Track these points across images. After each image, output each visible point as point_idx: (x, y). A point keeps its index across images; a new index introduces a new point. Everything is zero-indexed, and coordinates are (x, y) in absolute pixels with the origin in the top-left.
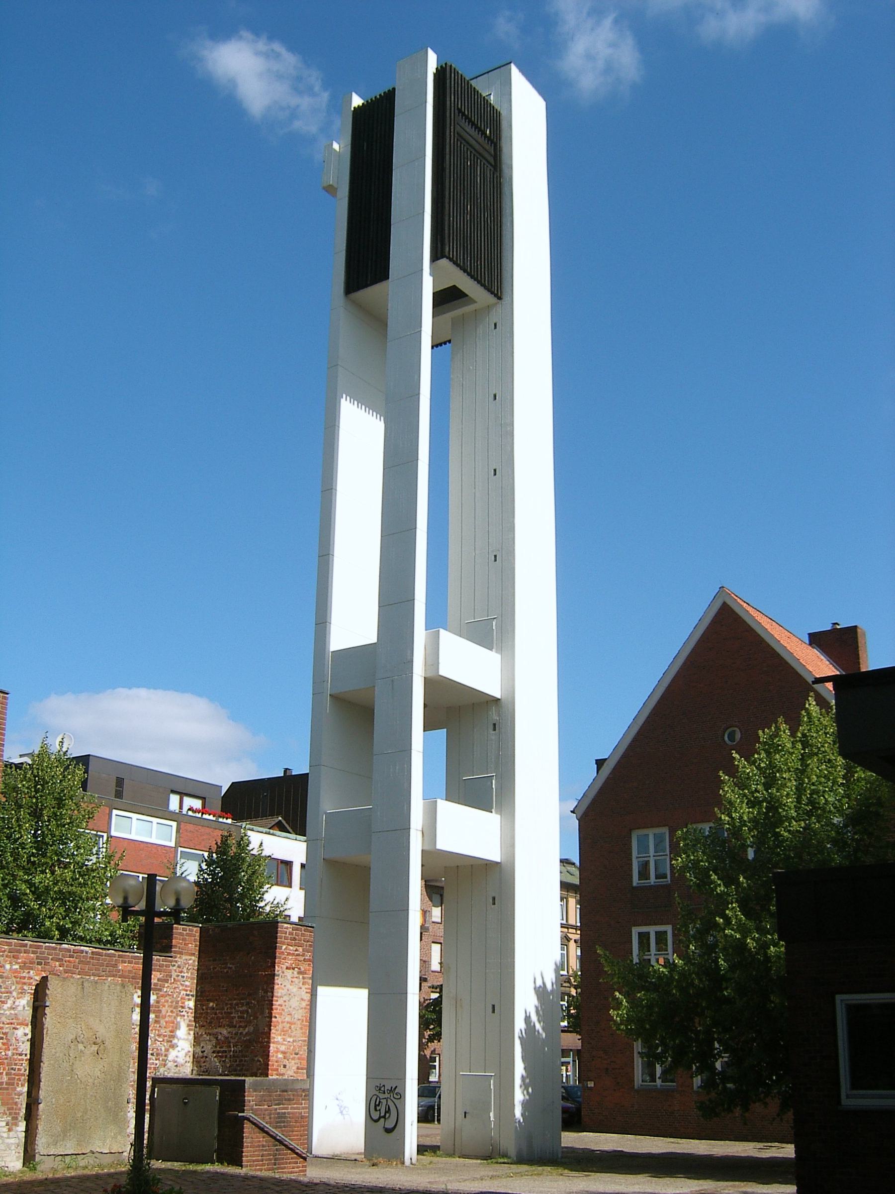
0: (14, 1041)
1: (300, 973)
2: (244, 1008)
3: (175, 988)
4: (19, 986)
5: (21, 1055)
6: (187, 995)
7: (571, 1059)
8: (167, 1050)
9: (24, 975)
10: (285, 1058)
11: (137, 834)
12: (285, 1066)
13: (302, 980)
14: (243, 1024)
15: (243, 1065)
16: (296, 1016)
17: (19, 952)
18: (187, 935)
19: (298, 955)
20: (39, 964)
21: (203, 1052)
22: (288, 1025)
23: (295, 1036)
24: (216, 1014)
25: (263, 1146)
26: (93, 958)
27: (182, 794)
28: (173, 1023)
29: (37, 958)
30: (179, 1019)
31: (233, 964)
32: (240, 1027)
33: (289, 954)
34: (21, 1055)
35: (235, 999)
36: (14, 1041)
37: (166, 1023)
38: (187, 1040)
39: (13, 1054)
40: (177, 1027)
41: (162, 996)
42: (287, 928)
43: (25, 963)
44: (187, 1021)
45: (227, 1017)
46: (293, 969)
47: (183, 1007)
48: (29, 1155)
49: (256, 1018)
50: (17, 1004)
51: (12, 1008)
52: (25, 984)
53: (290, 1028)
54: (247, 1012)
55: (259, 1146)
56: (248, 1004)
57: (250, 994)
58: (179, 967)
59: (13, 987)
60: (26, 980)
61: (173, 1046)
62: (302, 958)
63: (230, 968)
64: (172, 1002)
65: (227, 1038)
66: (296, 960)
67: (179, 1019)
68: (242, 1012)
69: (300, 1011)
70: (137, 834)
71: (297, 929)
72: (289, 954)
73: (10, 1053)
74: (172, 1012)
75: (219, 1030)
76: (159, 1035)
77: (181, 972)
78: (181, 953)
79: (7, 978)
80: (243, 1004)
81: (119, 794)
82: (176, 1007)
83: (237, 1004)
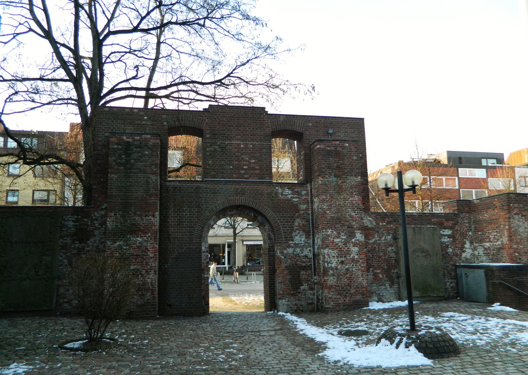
0: (388, 252)
1: (523, 216)
2: (495, 234)
3: (461, 227)
4: (386, 231)
5: (392, 258)
6: (468, 230)
7: (474, 190)
8: (461, 253)
9: (389, 226)
10: (520, 255)
11: (469, 175)
12: (520, 259)
13: (524, 219)
14: (495, 241)
15: (498, 259)
16: (523, 236)
17: (385, 218)
18: (464, 204)
19: (520, 208)
20: (395, 222)
21: (479, 253)
22: (519, 240)
23: (524, 245)
24: (482, 237)
25: (511, 296)
26: (419, 218)
27: (487, 158)
28: (462, 242)
29: (393, 219)
30: (465, 240)
31: (487, 215)
32: (494, 242)
33: (515, 208)
34: (392, 258)
35: (490, 230)
36: (388, 252)
37: (459, 242)
38: (471, 248)
39: (388, 258)
40: (465, 243)
41: (455, 231)
42: (512, 196)
43: (388, 222)
44: (469, 241)
45: (488, 238)
46: (519, 214)
47: (466, 235)
48: (414, 297)
49: (502, 238)
50: (387, 238)
51: (385, 240)
52: (389, 230)
53: (521, 241)
54: (497, 235)
55: (508, 296)
56: (497, 232)
57: (497, 227)
58: (462, 218)
59: (384, 232)
60: (390, 229)
61: (464, 252)
62: (523, 209)
63: (486, 217)
64: (460, 233)
65: (489, 247)
66: (520, 210)
67: (465, 240)
68: (494, 235)
69: (526, 233)
70: (469, 175)
71: (518, 196)
72: (515, 208)
73: (386, 257)
74: (461, 237)
75: (485, 244)
76: (456, 247)
77: (463, 220)
78: (462, 213)
79: (381, 228)
80: (494, 232)
81: (460, 163)
82: (463, 235)
83: (491, 232)
